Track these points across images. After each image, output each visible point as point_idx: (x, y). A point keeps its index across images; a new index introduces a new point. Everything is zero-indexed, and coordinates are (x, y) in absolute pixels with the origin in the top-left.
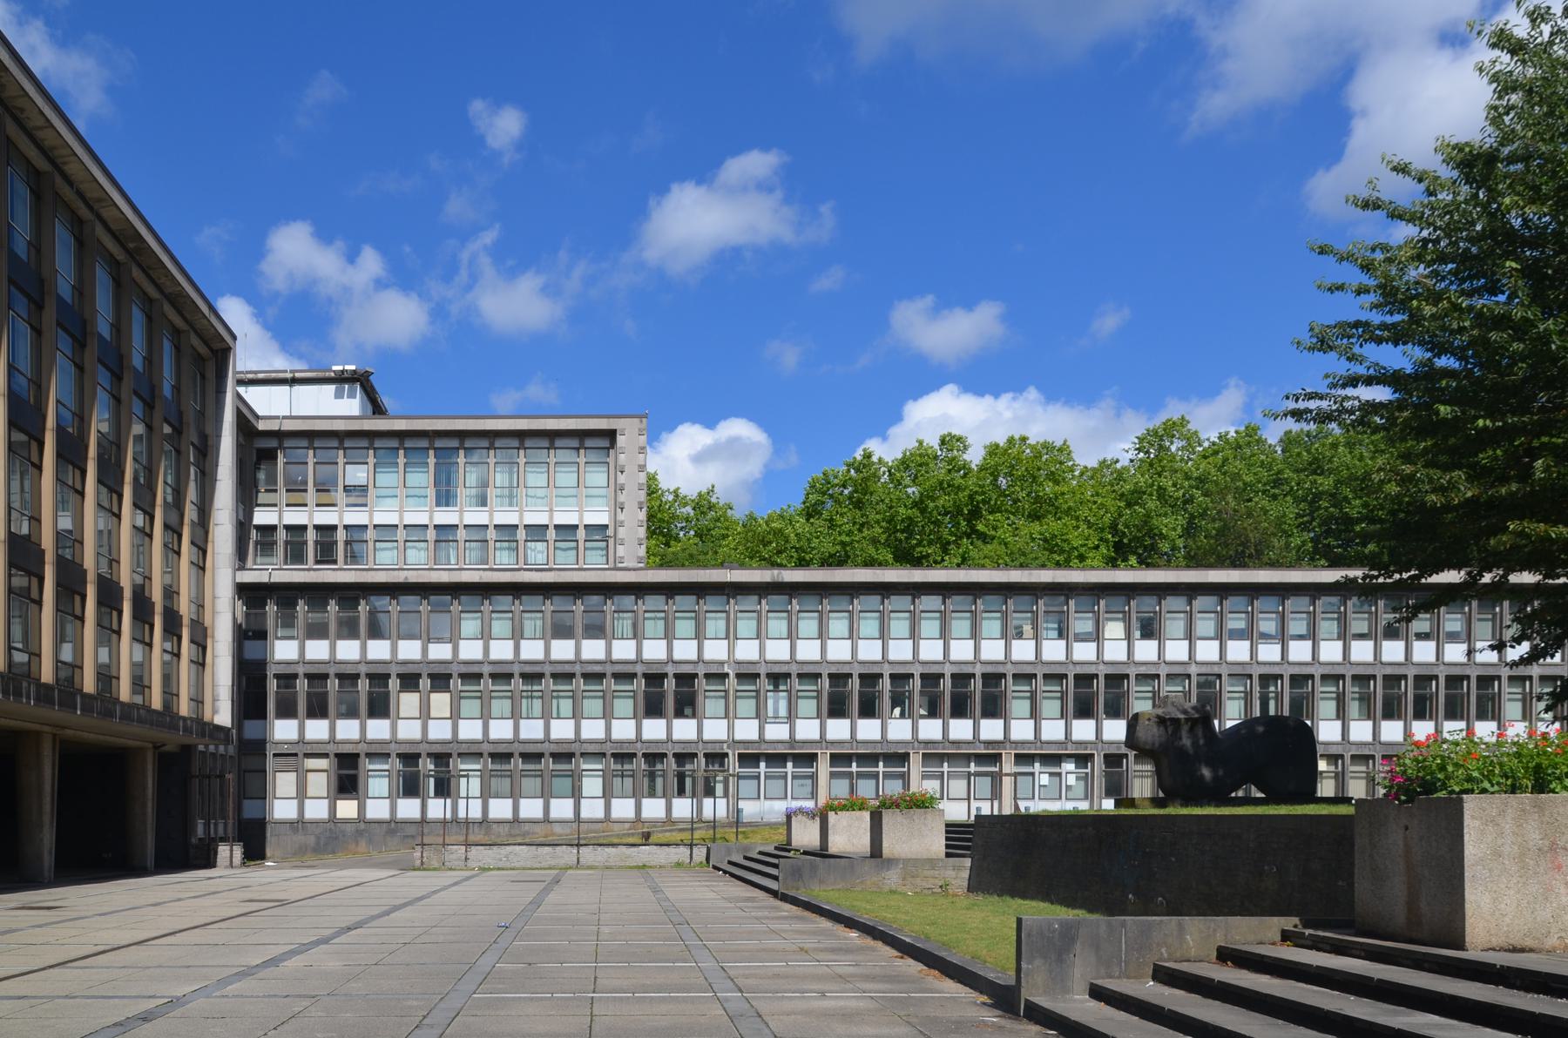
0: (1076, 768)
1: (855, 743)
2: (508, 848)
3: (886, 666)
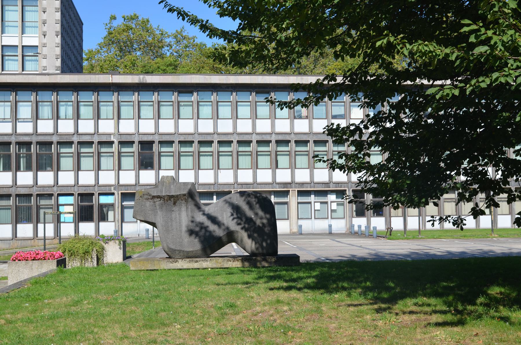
0: (337, 198)
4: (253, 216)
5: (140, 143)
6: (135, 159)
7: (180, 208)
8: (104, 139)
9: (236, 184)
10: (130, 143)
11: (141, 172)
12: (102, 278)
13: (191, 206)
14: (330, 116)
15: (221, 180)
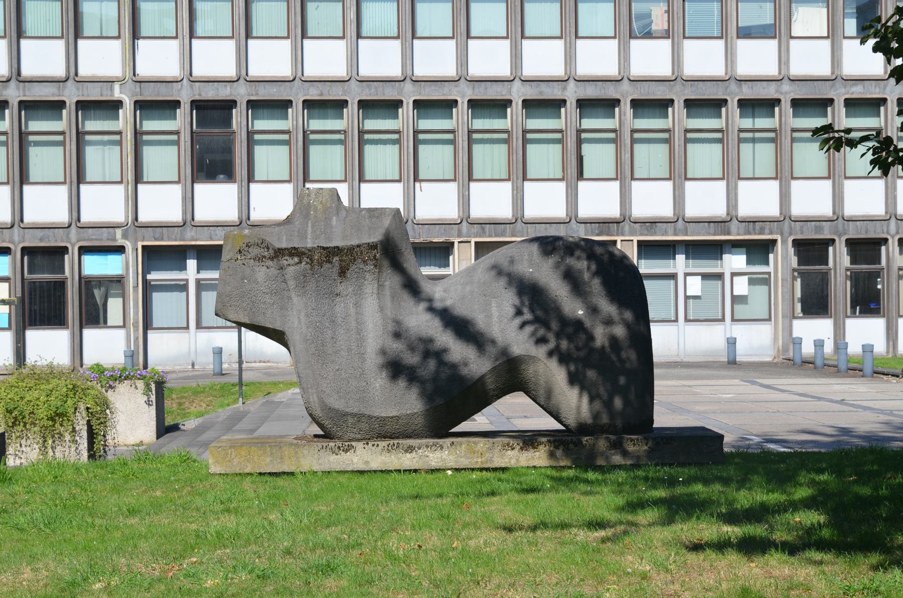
0: (749, 262)
1: (893, 221)
3: (408, 86)
4: (580, 312)
5: (197, 105)
6: (182, 152)
7: (360, 287)
8: (94, 93)
9: (464, 223)
10: (170, 107)
11: (198, 187)
12: (129, 500)
13: (392, 280)
14: (733, 31)
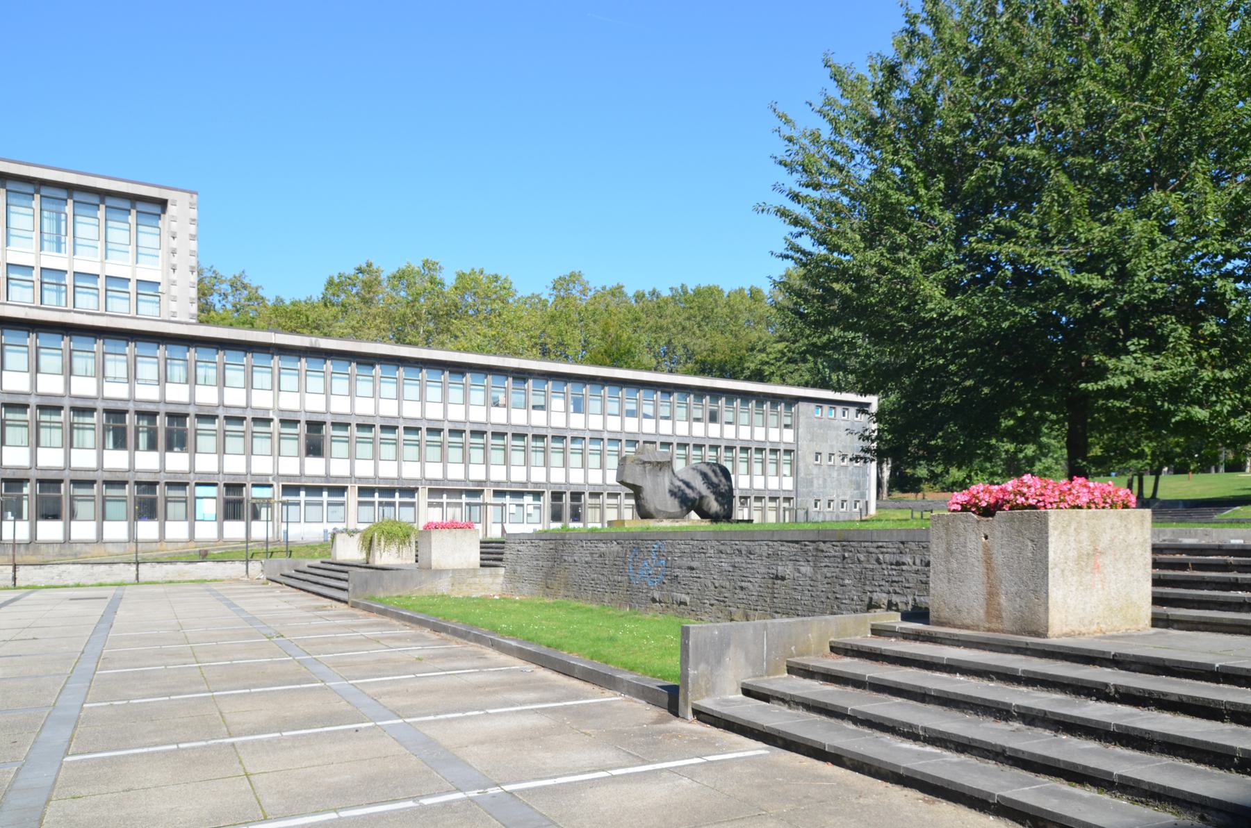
2: (60, 567)
3: (401, 420)
5: (308, 423)
14: (530, 407)
15: (405, 475)
